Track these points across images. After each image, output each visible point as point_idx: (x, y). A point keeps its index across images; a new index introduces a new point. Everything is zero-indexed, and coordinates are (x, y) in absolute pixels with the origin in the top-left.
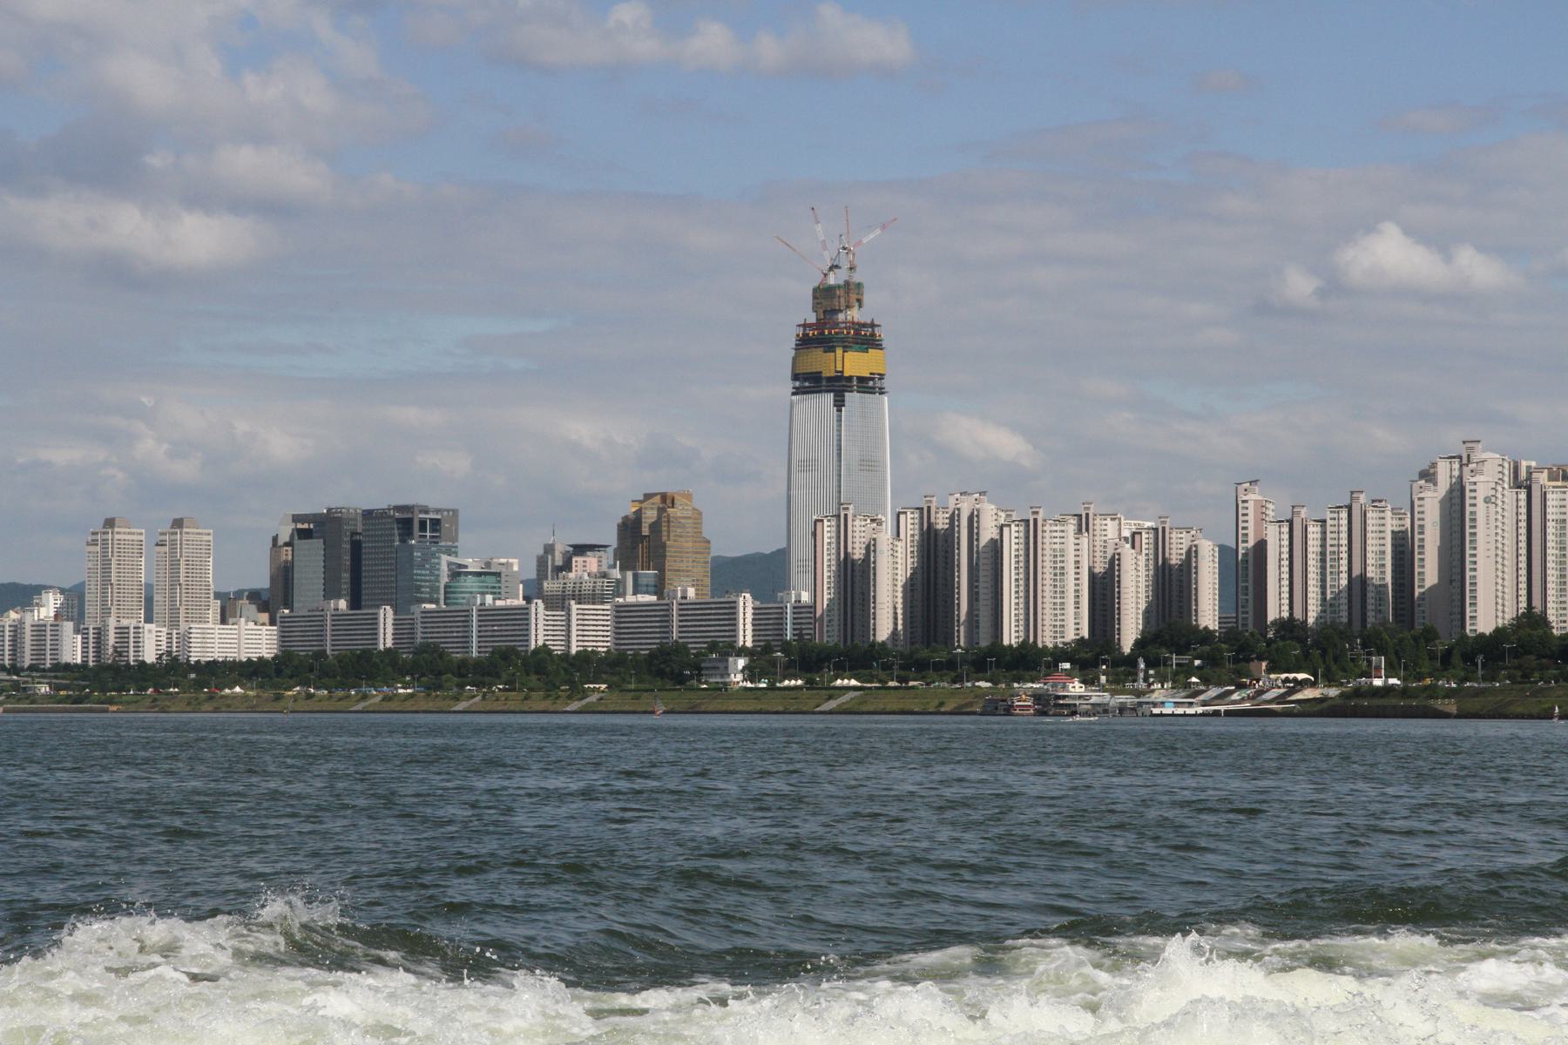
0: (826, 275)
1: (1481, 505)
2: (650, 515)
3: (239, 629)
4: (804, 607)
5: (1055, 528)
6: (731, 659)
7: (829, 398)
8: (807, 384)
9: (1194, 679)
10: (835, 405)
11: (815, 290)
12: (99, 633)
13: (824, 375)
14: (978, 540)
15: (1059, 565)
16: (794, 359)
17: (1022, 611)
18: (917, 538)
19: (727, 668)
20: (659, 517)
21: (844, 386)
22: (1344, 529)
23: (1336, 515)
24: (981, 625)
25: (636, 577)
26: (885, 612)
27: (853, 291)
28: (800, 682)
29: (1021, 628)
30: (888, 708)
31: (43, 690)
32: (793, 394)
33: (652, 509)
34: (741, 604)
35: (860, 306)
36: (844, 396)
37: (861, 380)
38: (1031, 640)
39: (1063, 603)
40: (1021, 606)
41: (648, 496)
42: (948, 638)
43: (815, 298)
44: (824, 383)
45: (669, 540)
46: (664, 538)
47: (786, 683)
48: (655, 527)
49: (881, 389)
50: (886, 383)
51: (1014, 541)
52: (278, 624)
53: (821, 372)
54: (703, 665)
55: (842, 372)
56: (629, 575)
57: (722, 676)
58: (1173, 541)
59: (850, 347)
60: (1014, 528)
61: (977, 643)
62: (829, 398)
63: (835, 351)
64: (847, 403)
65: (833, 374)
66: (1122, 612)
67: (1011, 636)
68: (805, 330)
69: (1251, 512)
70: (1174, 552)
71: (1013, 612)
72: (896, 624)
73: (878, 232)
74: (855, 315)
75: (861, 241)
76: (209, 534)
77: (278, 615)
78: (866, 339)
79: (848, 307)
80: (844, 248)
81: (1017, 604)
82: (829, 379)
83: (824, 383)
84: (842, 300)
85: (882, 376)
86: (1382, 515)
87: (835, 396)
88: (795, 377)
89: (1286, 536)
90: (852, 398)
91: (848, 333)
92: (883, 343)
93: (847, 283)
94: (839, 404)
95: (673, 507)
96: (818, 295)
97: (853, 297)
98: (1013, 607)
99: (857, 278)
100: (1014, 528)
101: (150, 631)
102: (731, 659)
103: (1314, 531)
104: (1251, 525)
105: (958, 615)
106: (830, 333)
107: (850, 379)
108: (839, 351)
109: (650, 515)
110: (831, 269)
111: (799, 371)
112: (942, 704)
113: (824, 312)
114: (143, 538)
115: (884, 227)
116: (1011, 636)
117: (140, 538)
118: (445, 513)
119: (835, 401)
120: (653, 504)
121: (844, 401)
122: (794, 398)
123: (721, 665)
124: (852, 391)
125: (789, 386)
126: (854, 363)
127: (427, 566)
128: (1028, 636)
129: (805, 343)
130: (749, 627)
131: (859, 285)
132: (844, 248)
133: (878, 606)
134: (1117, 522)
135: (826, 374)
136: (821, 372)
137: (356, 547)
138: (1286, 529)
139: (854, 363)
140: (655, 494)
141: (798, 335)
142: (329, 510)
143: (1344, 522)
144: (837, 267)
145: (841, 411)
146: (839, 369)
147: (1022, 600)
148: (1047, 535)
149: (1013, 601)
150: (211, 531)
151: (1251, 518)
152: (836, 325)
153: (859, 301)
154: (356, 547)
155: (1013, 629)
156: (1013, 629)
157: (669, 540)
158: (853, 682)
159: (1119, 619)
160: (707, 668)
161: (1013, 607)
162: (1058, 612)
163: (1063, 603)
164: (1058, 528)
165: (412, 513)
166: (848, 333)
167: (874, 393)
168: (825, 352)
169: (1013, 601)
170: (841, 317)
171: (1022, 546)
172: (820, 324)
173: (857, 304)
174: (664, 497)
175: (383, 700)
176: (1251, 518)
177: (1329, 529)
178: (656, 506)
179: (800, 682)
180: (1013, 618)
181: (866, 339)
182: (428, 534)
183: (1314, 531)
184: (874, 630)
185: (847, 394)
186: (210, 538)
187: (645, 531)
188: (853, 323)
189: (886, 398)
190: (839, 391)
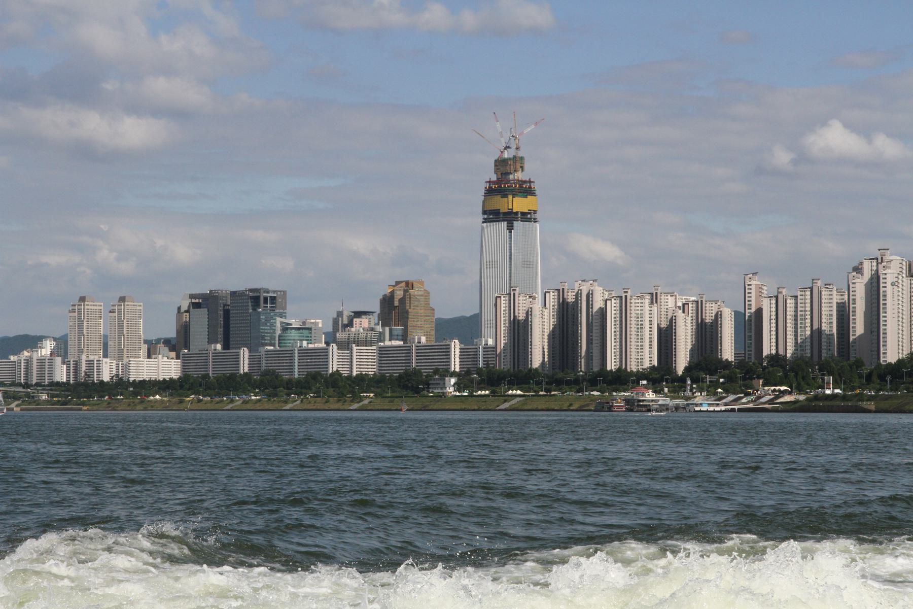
0: (502, 152)
1: (889, 285)
2: (399, 294)
3: (158, 362)
5: (637, 301)
6: (447, 379)
7: (504, 225)
8: (491, 216)
10: (508, 229)
11: (496, 161)
12: (76, 364)
13: (501, 211)
14: (592, 308)
15: (640, 323)
16: (484, 202)
18: (556, 307)
19: (444, 384)
20: (405, 295)
22: (808, 301)
24: (594, 358)
25: (391, 330)
27: (518, 162)
28: (487, 392)
29: (618, 360)
30: (540, 407)
31: (44, 397)
32: (483, 222)
33: (400, 290)
34: (453, 346)
35: (522, 171)
36: (513, 223)
37: (523, 214)
38: (624, 367)
40: (618, 347)
41: (398, 283)
42: (575, 366)
44: (501, 216)
45: (410, 308)
46: (407, 308)
48: (402, 301)
49: (535, 219)
50: (538, 216)
52: (181, 358)
53: (499, 210)
54: (430, 382)
55: (512, 209)
56: (387, 329)
57: (442, 389)
58: (707, 308)
60: (613, 301)
61: (592, 369)
62: (504, 225)
64: (515, 228)
65: (507, 211)
66: (677, 350)
69: (753, 291)
70: (707, 315)
71: (613, 351)
72: (544, 358)
73: (533, 127)
74: (519, 175)
75: (523, 132)
77: (181, 353)
78: (526, 190)
79: (515, 171)
80: (513, 136)
81: (615, 346)
82: (505, 214)
83: (501, 216)
84: (512, 167)
85: (535, 212)
86: (831, 293)
87: (508, 223)
88: (484, 212)
89: (774, 306)
90: (518, 224)
92: (536, 192)
93: (515, 157)
94: (510, 228)
95: (412, 289)
96: (498, 164)
97: (518, 165)
99: (520, 154)
100: (613, 301)
101: (106, 363)
102: (447, 379)
103: (790, 302)
104: (753, 299)
105: (581, 353)
106: (505, 186)
107: (517, 213)
108: (510, 197)
109: (399, 294)
110: (505, 149)
111: (488, 208)
112: (571, 405)
113: (501, 174)
115: (536, 124)
117: (100, 308)
119: (508, 226)
121: (513, 226)
123: (441, 382)
124: (518, 221)
126: (519, 204)
127: (268, 324)
129: (491, 191)
130: (457, 360)
131: (522, 158)
132: (513, 136)
134: (674, 297)
136: (499, 210)
137: (227, 313)
138: (774, 301)
139: (519, 204)
140: (402, 282)
141: (486, 188)
142: (211, 291)
143: (808, 297)
144: (509, 147)
145: (510, 232)
146: (510, 207)
147: (618, 344)
148: (633, 305)
149: (613, 344)
150: (142, 304)
151: (753, 295)
153: (522, 167)
154: (227, 313)
155: (613, 361)
156: (613, 361)
157: (410, 308)
158: (519, 392)
159: (675, 355)
164: (639, 301)
165: (260, 293)
166: (516, 186)
167: (531, 222)
168: (502, 197)
169: (613, 344)
170: (511, 177)
171: (618, 312)
172: (499, 181)
174: (407, 283)
175: (243, 403)
176: (753, 295)
177: (799, 301)
178: (402, 289)
179: (487, 392)
180: (613, 354)
181: (526, 190)
183: (790, 302)
184: (531, 361)
185: (515, 222)
187: (396, 303)
188: (518, 180)
189: (538, 225)
190: (510, 221)
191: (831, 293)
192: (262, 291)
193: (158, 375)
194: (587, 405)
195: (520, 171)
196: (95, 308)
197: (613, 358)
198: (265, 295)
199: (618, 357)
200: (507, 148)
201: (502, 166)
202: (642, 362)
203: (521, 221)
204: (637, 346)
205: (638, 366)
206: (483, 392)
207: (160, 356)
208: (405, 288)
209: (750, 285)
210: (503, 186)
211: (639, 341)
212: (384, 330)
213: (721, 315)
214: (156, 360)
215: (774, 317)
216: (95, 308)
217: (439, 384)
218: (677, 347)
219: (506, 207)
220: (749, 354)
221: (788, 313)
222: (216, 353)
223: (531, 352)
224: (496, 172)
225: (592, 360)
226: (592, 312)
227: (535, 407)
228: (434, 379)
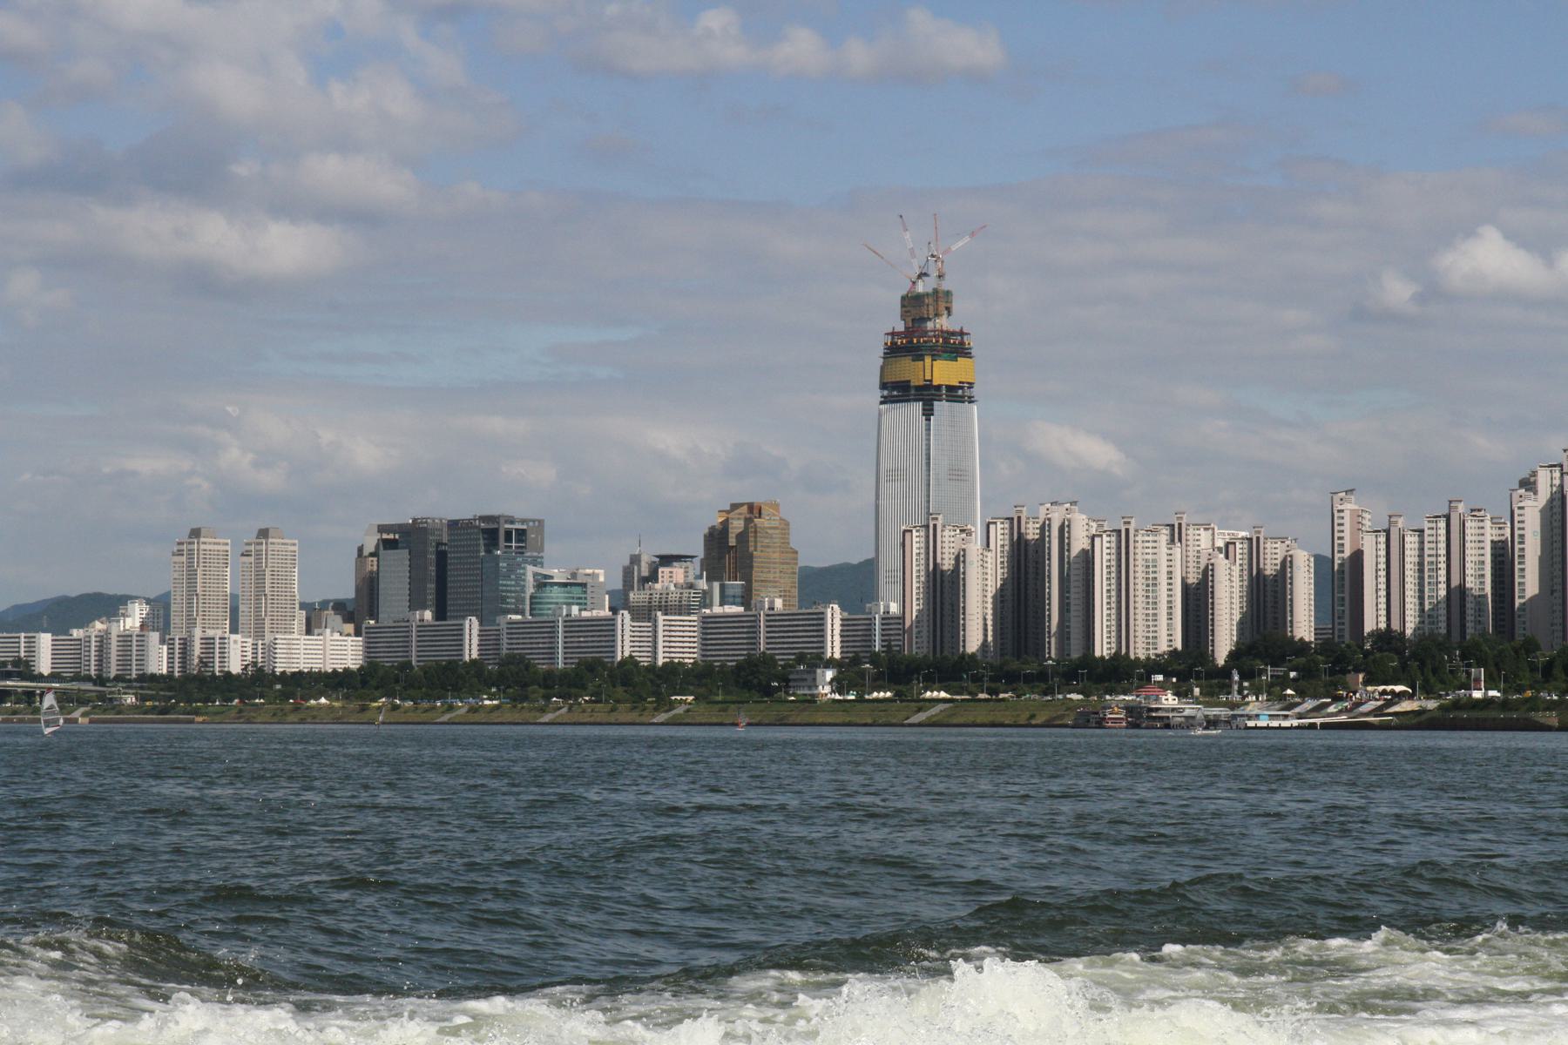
0: (914, 283)
2: (737, 525)
3: (325, 639)
4: (892, 618)
5: (1147, 538)
9: (1289, 692)
10: (923, 414)
11: (903, 298)
13: (912, 384)
14: (1069, 550)
15: (1151, 576)
16: (882, 368)
17: (1114, 623)
18: (1007, 548)
19: (815, 679)
21: (933, 395)
22: (1443, 538)
23: (1434, 525)
25: (722, 588)
26: (975, 617)
27: (941, 298)
28: (889, 694)
29: (1113, 640)
32: (882, 403)
33: (739, 519)
34: (829, 615)
35: (949, 314)
36: (932, 405)
37: (950, 388)
38: (1124, 651)
39: (1155, 615)
40: (1113, 617)
41: (735, 507)
42: (1039, 650)
43: (903, 306)
44: (913, 392)
46: (751, 549)
47: (875, 694)
48: (743, 537)
49: (970, 397)
50: (975, 392)
51: (1105, 551)
52: (364, 634)
53: (909, 381)
55: (931, 381)
56: (716, 585)
59: (940, 356)
60: (1105, 538)
61: (1069, 655)
63: (923, 360)
64: (935, 413)
65: (922, 383)
66: (1216, 623)
67: (1103, 647)
68: (893, 338)
69: (1347, 521)
70: (1268, 562)
72: (986, 635)
73: (967, 239)
74: (944, 323)
76: (294, 545)
77: (364, 626)
78: (955, 347)
79: (937, 315)
80: (933, 256)
81: (1109, 615)
82: (918, 388)
83: (913, 392)
84: (931, 308)
86: (1481, 524)
87: (923, 405)
88: (883, 386)
89: (1383, 546)
91: (937, 341)
93: (936, 291)
95: (760, 517)
96: (906, 303)
97: (942, 305)
98: (1105, 618)
101: (235, 642)
103: (1411, 541)
105: (1049, 627)
106: (918, 342)
107: (939, 387)
108: (928, 360)
109: (737, 525)
112: (1033, 716)
113: (913, 320)
114: (228, 548)
115: (973, 234)
116: (1103, 647)
118: (531, 524)
119: (924, 410)
120: (740, 514)
121: (932, 410)
122: (882, 407)
123: (809, 677)
125: (877, 394)
126: (943, 372)
127: (513, 577)
128: (1119, 647)
129: (893, 351)
130: (837, 639)
131: (948, 294)
132: (933, 256)
133: (967, 617)
135: (914, 383)
136: (909, 381)
138: (1382, 539)
139: (943, 372)
141: (886, 344)
143: (1443, 532)
144: (926, 275)
147: (1113, 611)
148: (1139, 545)
151: (1347, 521)
152: (925, 333)
153: (948, 309)
155: (1105, 640)
156: (1105, 640)
158: (943, 694)
159: (1213, 630)
160: (795, 680)
161: (1105, 618)
162: (1151, 623)
163: (1155, 615)
164: (1150, 538)
165: (498, 523)
166: (937, 341)
167: (963, 402)
168: (913, 360)
170: (930, 325)
172: (908, 333)
173: (946, 312)
174: (751, 507)
177: (1427, 539)
178: (743, 517)
179: (889, 694)
181: (955, 347)
182: (514, 544)
183: (1411, 541)
185: (935, 403)
186: (296, 548)
187: (732, 542)
191: (1481, 524)
192: (502, 521)
193: (324, 663)
194: (1062, 717)
195: (945, 316)
196: (216, 547)
197: (1105, 635)
198: (507, 526)
199: (1113, 634)
200: (922, 275)
201: (914, 305)
202: (1154, 644)
203: (947, 401)
204: (1147, 615)
205: (1148, 649)
206: (882, 694)
207: (328, 631)
208: (748, 516)
209: (1342, 511)
210: (915, 341)
211: (1151, 606)
212: (711, 588)
213: (1291, 562)
214: (321, 637)
215: (1382, 566)
216: (216, 547)
217: (806, 680)
218: (1216, 618)
219: (922, 377)
220: (1340, 630)
221: (1408, 559)
222: (422, 626)
223: (964, 625)
224: (903, 317)
225: (1069, 639)
226: (1069, 557)
227: (971, 719)
228: (797, 672)
